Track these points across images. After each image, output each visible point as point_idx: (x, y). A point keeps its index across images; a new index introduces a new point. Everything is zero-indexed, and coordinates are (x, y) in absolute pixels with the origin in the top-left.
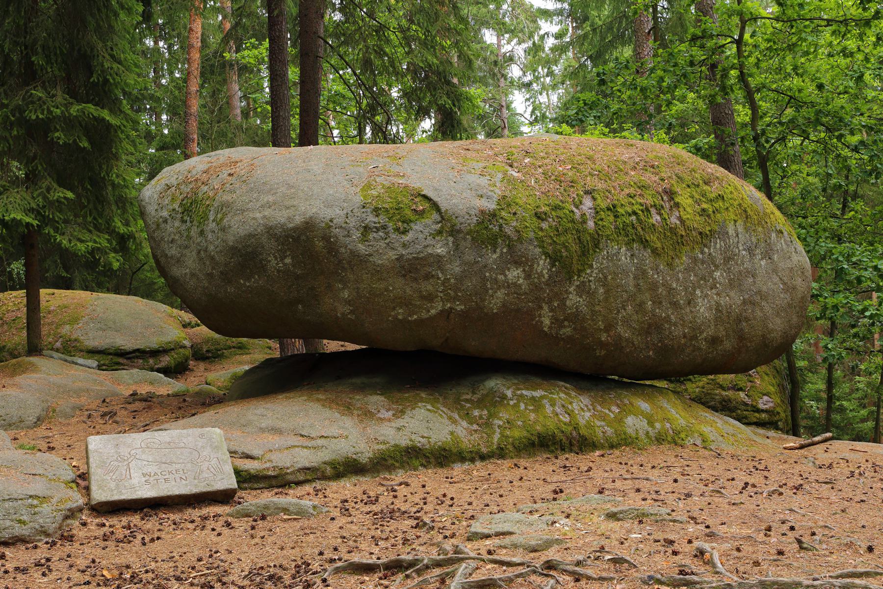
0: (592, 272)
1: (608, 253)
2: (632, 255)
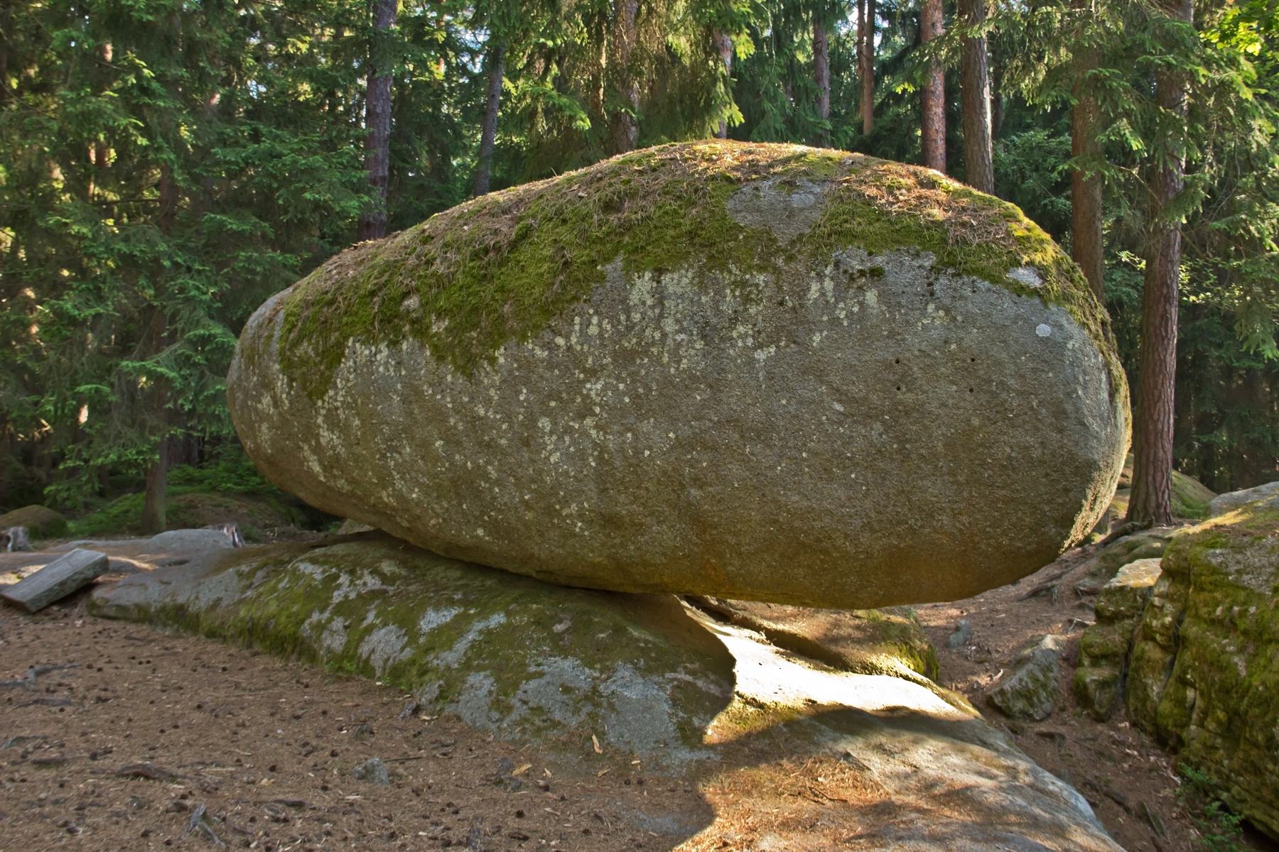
0: (336, 394)
1: (355, 362)
2: (398, 363)
